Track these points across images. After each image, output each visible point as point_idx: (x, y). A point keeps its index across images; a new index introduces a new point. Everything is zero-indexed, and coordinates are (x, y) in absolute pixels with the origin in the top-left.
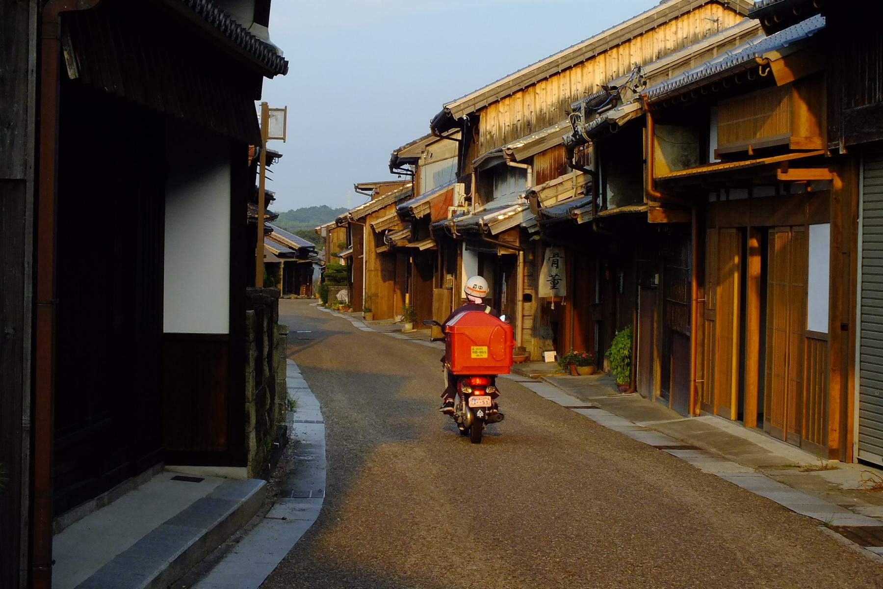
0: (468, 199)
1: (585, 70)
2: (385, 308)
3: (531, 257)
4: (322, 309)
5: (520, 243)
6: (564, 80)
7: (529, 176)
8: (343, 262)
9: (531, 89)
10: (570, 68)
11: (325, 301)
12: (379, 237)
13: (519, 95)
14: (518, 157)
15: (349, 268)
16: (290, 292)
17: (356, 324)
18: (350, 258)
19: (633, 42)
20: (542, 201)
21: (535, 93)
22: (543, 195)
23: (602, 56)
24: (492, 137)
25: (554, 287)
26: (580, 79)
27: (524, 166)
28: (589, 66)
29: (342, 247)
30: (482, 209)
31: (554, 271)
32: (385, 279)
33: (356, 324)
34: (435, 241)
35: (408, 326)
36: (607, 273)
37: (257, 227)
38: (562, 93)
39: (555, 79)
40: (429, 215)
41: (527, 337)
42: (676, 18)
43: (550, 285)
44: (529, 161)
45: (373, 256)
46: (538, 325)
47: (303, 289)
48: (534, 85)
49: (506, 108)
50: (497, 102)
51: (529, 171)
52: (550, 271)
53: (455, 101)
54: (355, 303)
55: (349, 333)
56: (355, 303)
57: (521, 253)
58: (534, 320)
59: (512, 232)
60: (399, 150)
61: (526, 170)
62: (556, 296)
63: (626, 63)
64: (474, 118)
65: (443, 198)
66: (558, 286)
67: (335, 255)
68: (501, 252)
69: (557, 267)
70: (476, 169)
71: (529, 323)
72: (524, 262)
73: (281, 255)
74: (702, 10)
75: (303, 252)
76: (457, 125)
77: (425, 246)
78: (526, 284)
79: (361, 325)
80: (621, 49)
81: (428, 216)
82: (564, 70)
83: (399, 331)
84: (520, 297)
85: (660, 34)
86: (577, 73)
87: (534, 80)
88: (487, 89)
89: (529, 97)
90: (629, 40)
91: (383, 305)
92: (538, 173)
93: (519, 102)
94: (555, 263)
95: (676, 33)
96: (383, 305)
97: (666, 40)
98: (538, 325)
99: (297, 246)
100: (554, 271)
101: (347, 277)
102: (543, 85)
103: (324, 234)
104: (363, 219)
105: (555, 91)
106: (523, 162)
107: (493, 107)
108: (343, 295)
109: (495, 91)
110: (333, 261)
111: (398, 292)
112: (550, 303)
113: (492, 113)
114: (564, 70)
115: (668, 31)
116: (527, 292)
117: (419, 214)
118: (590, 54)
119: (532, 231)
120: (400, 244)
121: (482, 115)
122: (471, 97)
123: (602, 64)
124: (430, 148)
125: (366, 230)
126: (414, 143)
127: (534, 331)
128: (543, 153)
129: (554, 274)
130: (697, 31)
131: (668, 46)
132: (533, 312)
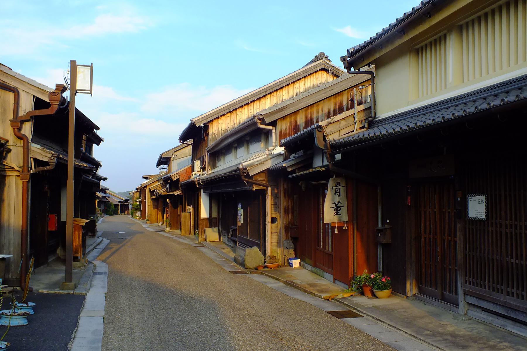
0: (203, 169)
1: (261, 103)
2: (154, 219)
3: (276, 191)
4: (131, 218)
5: (268, 181)
6: (251, 107)
7: (274, 135)
8: (138, 203)
9: (234, 112)
10: (254, 101)
11: (133, 216)
12: (152, 193)
13: (229, 115)
14: (267, 121)
15: (140, 205)
16: (122, 213)
17: (144, 226)
18: (140, 202)
19: (284, 88)
20: (328, 135)
21: (237, 114)
22: (328, 130)
23: (269, 96)
24: (215, 136)
25: (337, 213)
26: (258, 107)
27: (270, 128)
28: (263, 101)
29: (138, 199)
30: (211, 172)
31: (337, 199)
32: (154, 208)
33: (144, 226)
34: (182, 191)
35: (168, 229)
36: (409, 198)
37: (67, 166)
38: (250, 114)
39: (246, 107)
40: (179, 179)
41: (274, 248)
42: (305, 77)
43: (333, 212)
44: (274, 124)
45: (150, 200)
46: (282, 239)
47: (126, 212)
48: (236, 109)
49: (222, 121)
50: (218, 118)
51: (274, 131)
52: (333, 199)
53: (196, 117)
54: (143, 216)
55: (143, 232)
56: (143, 216)
57: (269, 188)
58: (279, 236)
59: (262, 174)
60: (163, 154)
61: (271, 131)
62: (339, 222)
63: (281, 99)
64: (206, 126)
65: (185, 171)
66: (340, 212)
67: (135, 201)
68: (255, 188)
69: (339, 195)
70: (208, 152)
71: (275, 238)
72: (272, 195)
73: (119, 202)
74: (317, 74)
75: (126, 201)
76: (195, 134)
77: (177, 193)
78: (273, 210)
79: (146, 226)
80: (278, 92)
81: (178, 179)
82: (251, 102)
83: (164, 231)
84: (269, 219)
85: (297, 85)
86: (257, 104)
87: (237, 107)
88: (213, 111)
89: (233, 116)
90: (282, 88)
91: (153, 218)
92: (280, 133)
93: (229, 118)
94: (337, 192)
95: (305, 84)
96: (153, 218)
97: (300, 88)
98: (282, 239)
99: (124, 199)
100: (337, 199)
101: (140, 208)
102: (240, 109)
103: (132, 194)
104: (146, 187)
105: (246, 113)
106: (270, 124)
107: (215, 121)
108: (138, 214)
109: (217, 112)
110: (135, 203)
111: (160, 213)
112: (333, 228)
113: (215, 123)
114: (251, 102)
115: (301, 84)
116: (274, 216)
117: (174, 179)
118: (264, 94)
119: (289, 170)
120: (163, 194)
121: (210, 124)
122: (205, 115)
123: (269, 99)
124: (176, 153)
125: (147, 191)
126: (169, 151)
127: (279, 243)
128: (283, 118)
129: (337, 202)
130: (315, 84)
131: (301, 91)
132: (278, 230)
